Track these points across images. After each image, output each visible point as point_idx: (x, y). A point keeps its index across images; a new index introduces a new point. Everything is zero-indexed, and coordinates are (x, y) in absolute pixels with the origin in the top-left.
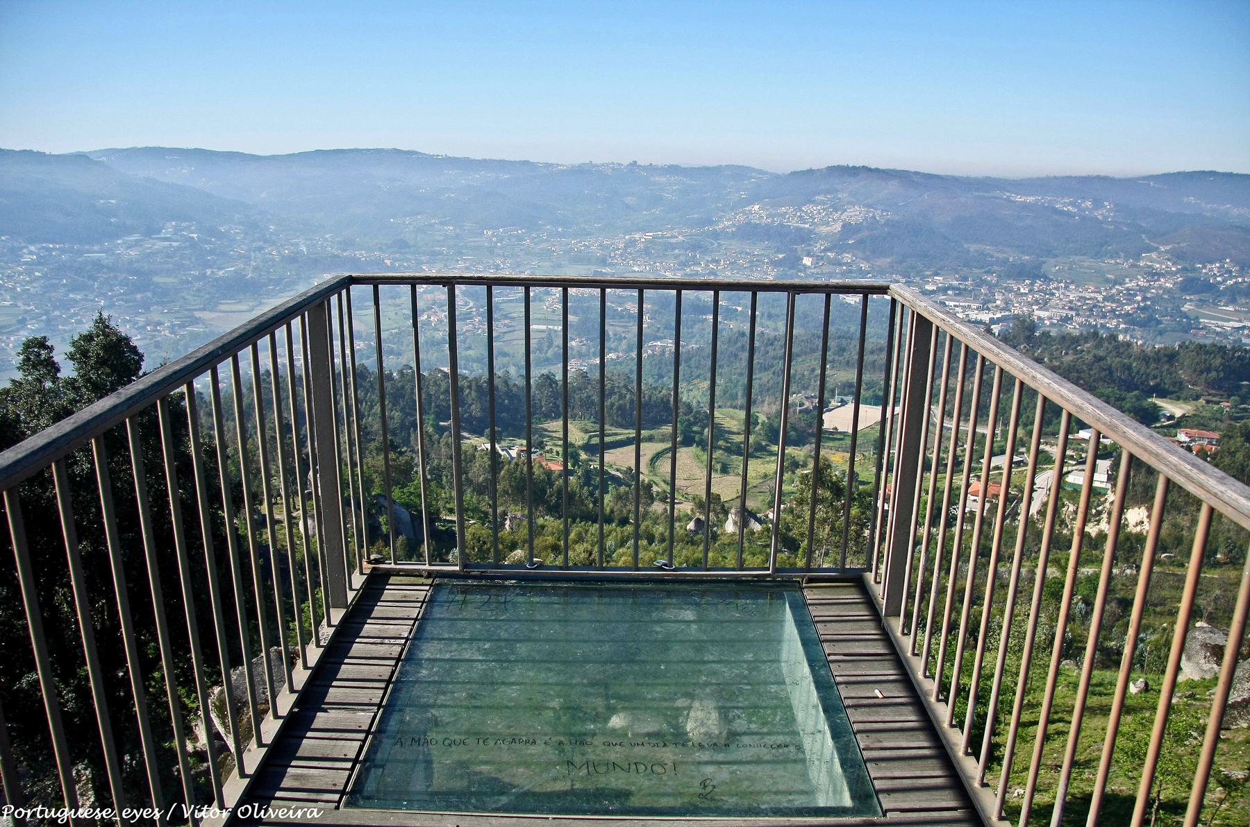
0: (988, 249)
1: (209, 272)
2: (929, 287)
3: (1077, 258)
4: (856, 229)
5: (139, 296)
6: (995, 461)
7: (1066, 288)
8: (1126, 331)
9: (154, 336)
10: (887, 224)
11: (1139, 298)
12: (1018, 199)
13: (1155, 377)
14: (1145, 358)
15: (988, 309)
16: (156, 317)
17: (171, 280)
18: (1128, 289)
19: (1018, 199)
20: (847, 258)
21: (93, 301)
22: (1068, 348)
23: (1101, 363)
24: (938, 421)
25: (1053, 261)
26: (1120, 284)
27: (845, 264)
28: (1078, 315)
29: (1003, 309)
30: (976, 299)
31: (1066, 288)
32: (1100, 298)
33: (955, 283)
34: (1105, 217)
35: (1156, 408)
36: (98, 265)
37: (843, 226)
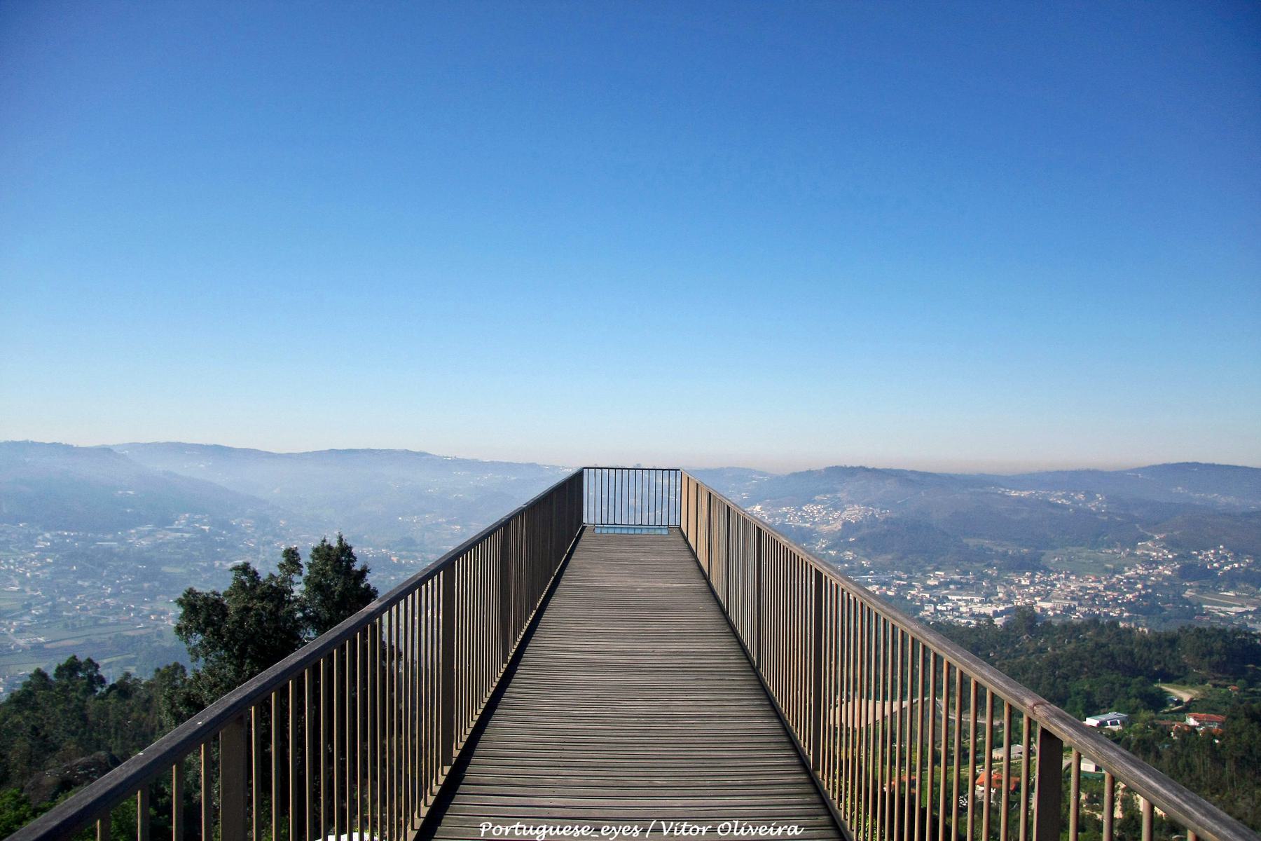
0: (986, 543)
1: (217, 563)
2: (931, 582)
3: (1074, 549)
4: (857, 526)
5: (146, 585)
6: (995, 754)
7: (1067, 578)
8: (1129, 619)
9: (157, 625)
10: (886, 521)
11: (1139, 586)
12: (1013, 493)
13: (1159, 662)
14: (1146, 643)
15: (991, 602)
16: (160, 606)
17: (179, 570)
18: (1127, 578)
19: (1013, 493)
20: (849, 555)
21: (100, 588)
22: (1070, 637)
23: (1103, 650)
24: (943, 713)
25: (1049, 552)
26: (1120, 573)
27: (847, 562)
28: (1080, 605)
29: (1005, 602)
30: (978, 593)
31: (1067, 578)
32: (1101, 587)
33: (956, 577)
34: (1098, 509)
35: (1164, 694)
36: (110, 553)
37: (844, 525)
